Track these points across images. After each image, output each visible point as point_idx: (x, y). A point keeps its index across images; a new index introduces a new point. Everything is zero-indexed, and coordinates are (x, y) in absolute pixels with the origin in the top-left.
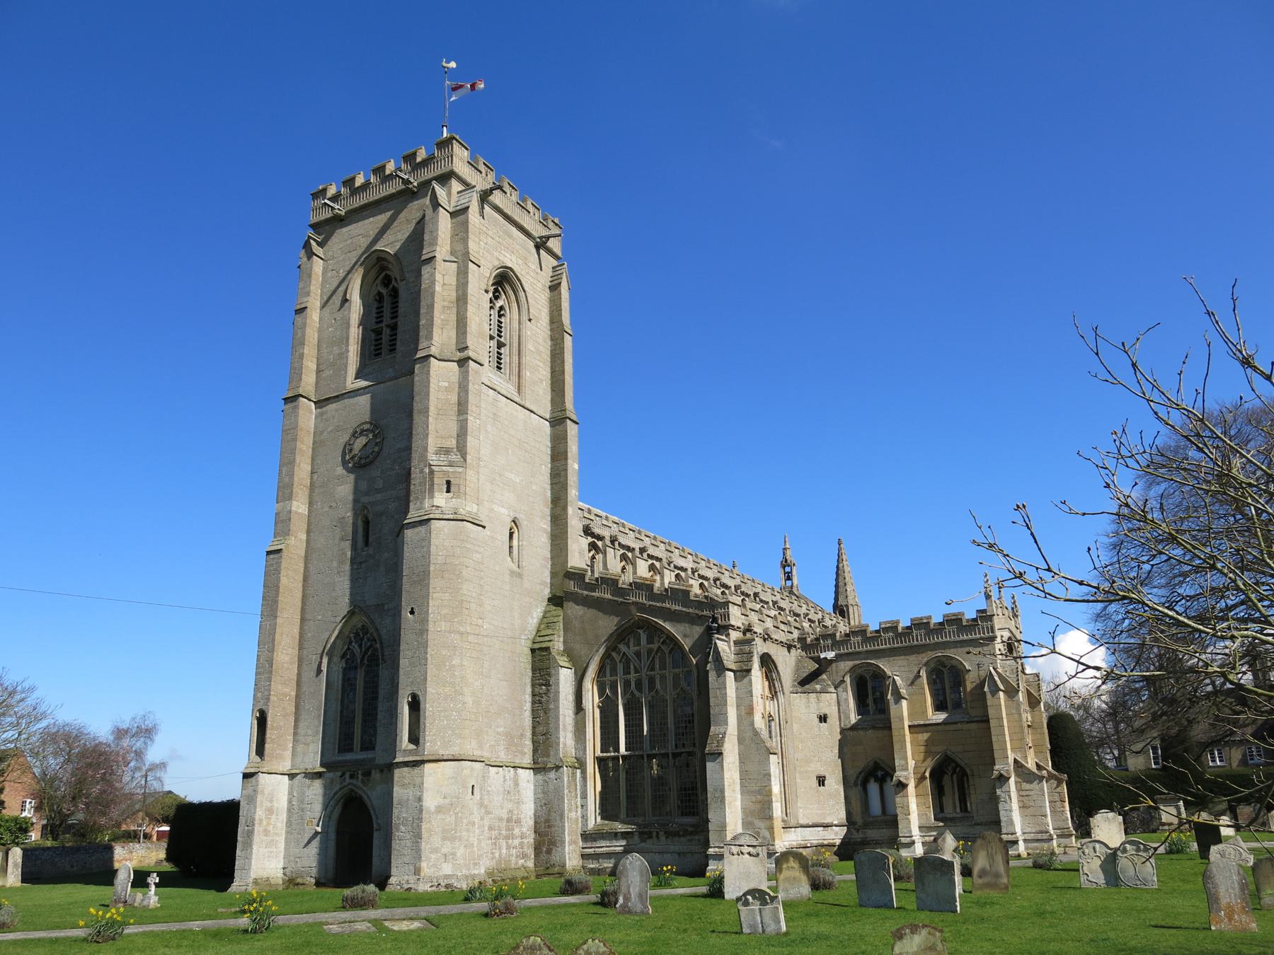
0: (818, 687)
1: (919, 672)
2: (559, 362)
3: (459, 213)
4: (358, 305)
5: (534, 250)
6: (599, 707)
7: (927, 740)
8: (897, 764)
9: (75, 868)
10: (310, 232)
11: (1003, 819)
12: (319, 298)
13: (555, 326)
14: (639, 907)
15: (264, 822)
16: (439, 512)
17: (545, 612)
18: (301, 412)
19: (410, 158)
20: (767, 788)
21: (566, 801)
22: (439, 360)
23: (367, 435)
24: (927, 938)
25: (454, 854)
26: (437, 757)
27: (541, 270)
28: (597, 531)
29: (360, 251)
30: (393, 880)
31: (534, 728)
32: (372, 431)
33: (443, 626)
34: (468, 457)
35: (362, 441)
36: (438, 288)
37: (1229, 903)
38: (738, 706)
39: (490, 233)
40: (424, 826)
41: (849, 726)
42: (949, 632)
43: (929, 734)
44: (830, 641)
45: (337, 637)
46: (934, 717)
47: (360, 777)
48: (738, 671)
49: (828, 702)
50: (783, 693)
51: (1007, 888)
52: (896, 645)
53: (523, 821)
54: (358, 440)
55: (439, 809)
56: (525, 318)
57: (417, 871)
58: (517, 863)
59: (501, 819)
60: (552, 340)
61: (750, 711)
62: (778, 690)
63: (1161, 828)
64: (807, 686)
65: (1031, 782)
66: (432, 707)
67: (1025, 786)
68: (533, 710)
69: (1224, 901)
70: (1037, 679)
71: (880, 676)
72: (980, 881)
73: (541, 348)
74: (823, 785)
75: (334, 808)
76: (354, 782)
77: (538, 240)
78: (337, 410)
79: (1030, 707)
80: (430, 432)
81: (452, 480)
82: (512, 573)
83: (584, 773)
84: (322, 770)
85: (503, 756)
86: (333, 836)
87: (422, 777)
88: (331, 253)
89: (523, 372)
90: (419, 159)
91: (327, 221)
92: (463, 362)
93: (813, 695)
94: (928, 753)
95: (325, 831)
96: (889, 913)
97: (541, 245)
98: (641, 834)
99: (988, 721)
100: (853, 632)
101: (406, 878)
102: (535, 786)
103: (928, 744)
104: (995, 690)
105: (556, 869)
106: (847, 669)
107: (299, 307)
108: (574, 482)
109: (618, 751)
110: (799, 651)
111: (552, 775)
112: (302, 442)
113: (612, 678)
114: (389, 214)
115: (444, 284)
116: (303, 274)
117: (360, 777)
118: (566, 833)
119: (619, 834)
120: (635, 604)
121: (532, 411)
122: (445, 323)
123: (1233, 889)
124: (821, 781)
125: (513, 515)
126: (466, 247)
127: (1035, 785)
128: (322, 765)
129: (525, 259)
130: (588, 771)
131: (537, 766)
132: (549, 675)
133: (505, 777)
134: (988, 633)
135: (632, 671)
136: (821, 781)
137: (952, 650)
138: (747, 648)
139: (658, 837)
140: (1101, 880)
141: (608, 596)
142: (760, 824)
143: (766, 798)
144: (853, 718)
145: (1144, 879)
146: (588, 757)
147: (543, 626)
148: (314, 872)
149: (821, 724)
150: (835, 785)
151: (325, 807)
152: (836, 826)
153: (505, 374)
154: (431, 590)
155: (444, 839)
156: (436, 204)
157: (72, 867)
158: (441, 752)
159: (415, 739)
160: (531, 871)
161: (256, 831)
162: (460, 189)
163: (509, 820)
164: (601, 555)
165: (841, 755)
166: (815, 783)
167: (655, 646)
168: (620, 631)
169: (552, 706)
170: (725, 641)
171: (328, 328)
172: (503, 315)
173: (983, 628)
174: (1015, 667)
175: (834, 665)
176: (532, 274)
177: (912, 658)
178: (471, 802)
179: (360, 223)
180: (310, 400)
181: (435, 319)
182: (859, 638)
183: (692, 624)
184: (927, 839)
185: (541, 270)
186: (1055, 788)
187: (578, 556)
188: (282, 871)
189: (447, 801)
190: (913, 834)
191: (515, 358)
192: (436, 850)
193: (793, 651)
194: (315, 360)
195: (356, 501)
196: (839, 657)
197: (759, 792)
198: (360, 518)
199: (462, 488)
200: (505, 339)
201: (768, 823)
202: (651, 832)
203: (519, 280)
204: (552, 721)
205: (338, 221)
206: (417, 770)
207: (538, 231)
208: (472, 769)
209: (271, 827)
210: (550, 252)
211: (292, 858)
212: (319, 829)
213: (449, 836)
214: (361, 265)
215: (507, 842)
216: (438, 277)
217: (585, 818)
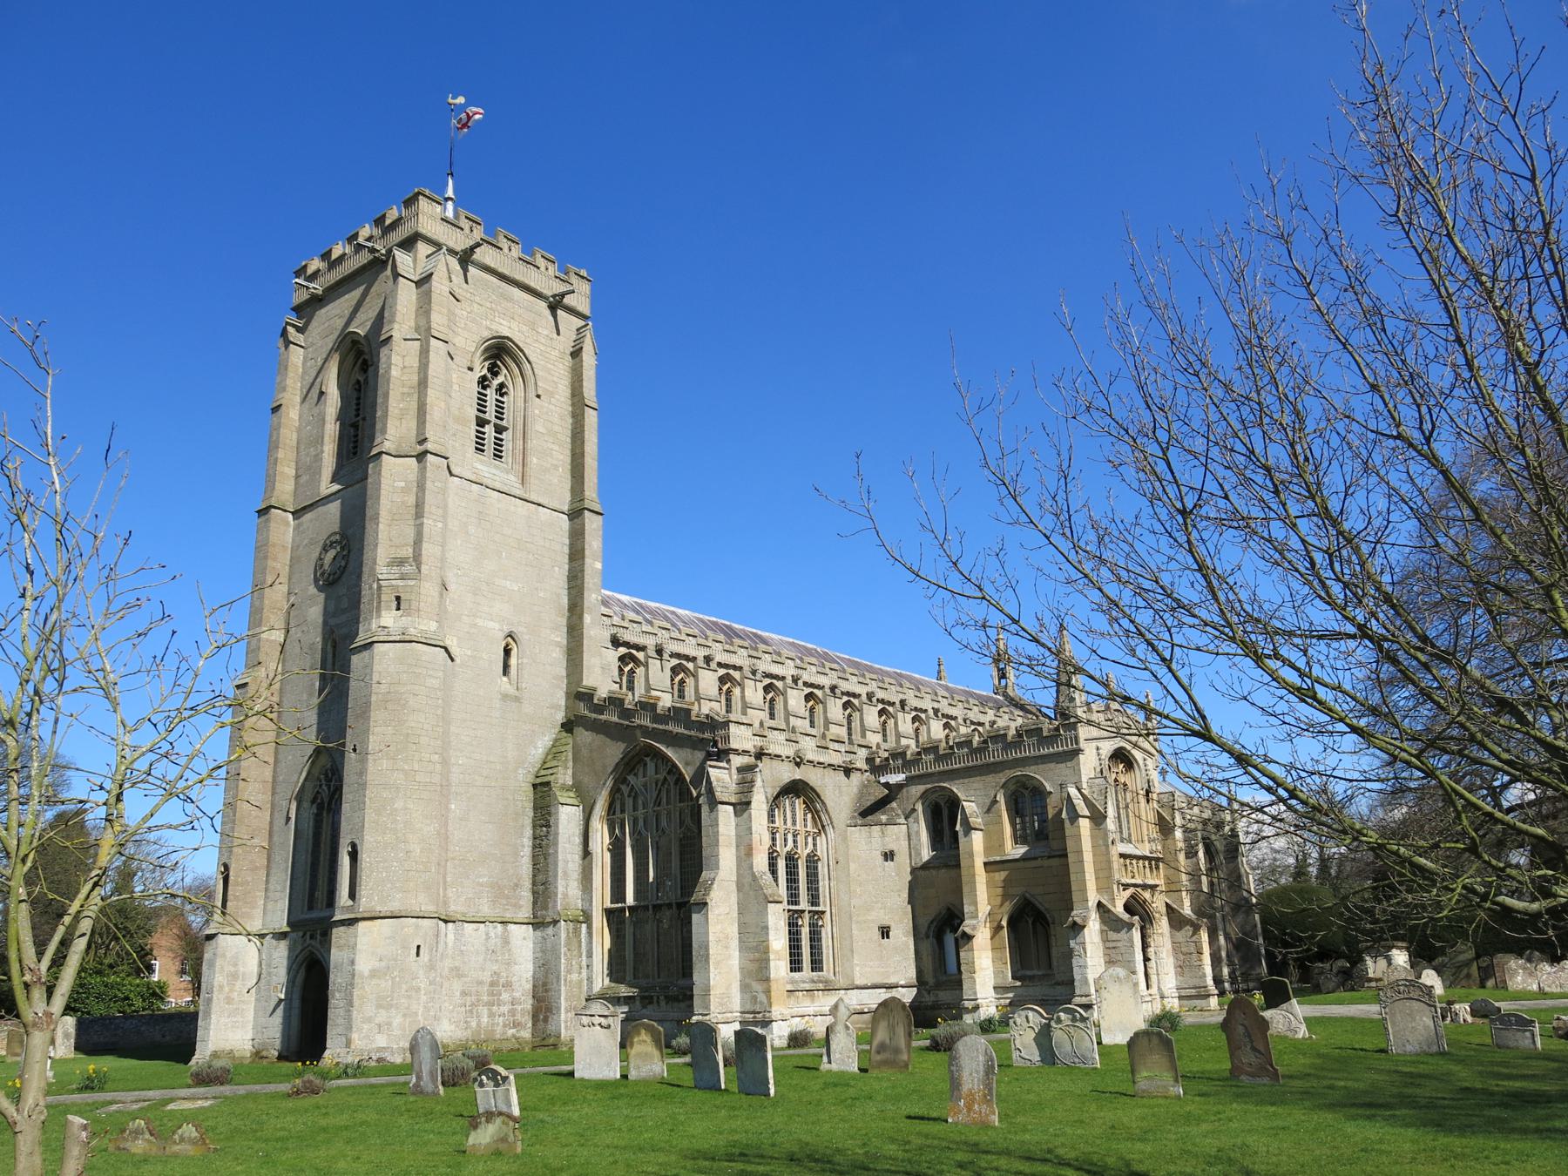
0: (884, 818)
1: (995, 797)
2: (579, 442)
3: (424, 281)
4: (335, 397)
5: (547, 312)
6: (609, 849)
7: (1004, 881)
8: (966, 911)
9: (168, 1038)
10: (292, 318)
11: (1077, 977)
12: (299, 392)
13: (576, 399)
14: (430, 1088)
15: (226, 989)
16: (385, 633)
17: (556, 740)
18: (272, 525)
19: (379, 221)
20: (765, 944)
21: (563, 961)
22: (395, 456)
23: (335, 548)
24: (500, 1128)
25: (389, 1024)
26: (373, 915)
27: (558, 334)
28: (627, 636)
29: (337, 333)
30: (327, 1054)
31: (534, 876)
32: (340, 543)
33: (385, 764)
34: (424, 568)
35: (331, 554)
36: (394, 372)
37: (970, 1090)
38: (737, 846)
39: (477, 299)
40: (356, 993)
41: (919, 865)
42: (1029, 745)
43: (1006, 873)
44: (900, 762)
45: (306, 779)
46: (1014, 852)
47: (318, 937)
48: (738, 804)
49: (896, 836)
50: (833, 827)
51: (906, 1066)
52: (971, 764)
53: (516, 986)
54: (328, 554)
55: (374, 974)
56: (532, 394)
57: (348, 1044)
58: (504, 1033)
59: (480, 983)
60: (573, 417)
61: (749, 852)
62: (825, 823)
63: (1366, 985)
64: (869, 817)
65: (1118, 931)
66: (370, 857)
67: (1112, 935)
68: (533, 856)
69: (965, 1088)
70: (1171, 798)
71: (954, 804)
72: (878, 1058)
73: (556, 428)
74: (888, 937)
75: (298, 972)
76: (313, 943)
77: (551, 299)
78: (311, 521)
79: (1162, 834)
80: (380, 541)
81: (402, 595)
82: (505, 697)
83: (590, 928)
84: (288, 929)
85: (486, 910)
86: (296, 1003)
87: (356, 937)
88: (310, 340)
89: (528, 459)
90: (388, 222)
91: (307, 303)
92: (421, 457)
93: (877, 828)
94: (1005, 896)
95: (288, 1000)
96: (716, 1094)
97: (556, 304)
98: (643, 998)
99: (1066, 856)
100: (924, 749)
101: (338, 1050)
102: (534, 943)
103: (1007, 884)
104: (1074, 816)
105: (551, 1041)
106: (919, 794)
107: (275, 405)
108: (594, 584)
109: (624, 901)
110: (868, 774)
111: (550, 930)
112: (275, 559)
113: (622, 816)
114: (363, 287)
115: (405, 367)
116: (282, 367)
117: (318, 937)
118: (562, 998)
119: (622, 999)
120: (641, 726)
121: (539, 505)
122: (403, 414)
123: (977, 1072)
124: (885, 932)
125: (506, 630)
126: (429, 322)
127: (1123, 935)
128: (289, 924)
129: (533, 326)
130: (594, 926)
131: (537, 921)
132: (549, 814)
133: (487, 934)
134: (1072, 745)
135: (641, 807)
136: (885, 932)
137: (1032, 767)
138: (749, 776)
139: (658, 1002)
140: (1036, 1057)
141: (615, 719)
142: (757, 987)
143: (764, 956)
144: (926, 854)
145: (1082, 1055)
146: (594, 909)
147: (550, 757)
148: (278, 1044)
149: (886, 863)
150: (903, 937)
151: (289, 970)
152: (902, 987)
153: (507, 463)
154: (371, 723)
155: (379, 1006)
156: (396, 275)
157: (164, 1036)
158: (378, 908)
159: (352, 895)
160: (526, 1042)
161: (215, 998)
162: (430, 252)
163: (492, 984)
164: (642, 668)
165: (912, 900)
166: (877, 934)
167: (661, 777)
168: (626, 760)
169: (551, 851)
170: (724, 768)
171: (306, 427)
172: (506, 393)
173: (1066, 739)
174: (1104, 787)
175: (905, 790)
176: (543, 341)
177: (990, 778)
178: (417, 966)
179: (337, 302)
180: (286, 511)
181: (390, 409)
182: (932, 756)
183: (694, 749)
184: (1002, 1002)
185: (558, 334)
186: (1192, 936)
187: (601, 675)
188: (251, 1043)
189: (383, 964)
190: (979, 996)
191: (520, 443)
192: (369, 1020)
193: (855, 776)
194: (293, 464)
195: (325, 623)
196: (911, 781)
197: (756, 949)
198: (329, 644)
199: (414, 605)
200: (508, 421)
201: (765, 985)
202: (652, 997)
203: (522, 351)
204: (551, 867)
205: (316, 302)
206: (352, 929)
207: (552, 287)
208: (417, 926)
209: (236, 994)
210: (571, 311)
211: (259, 1029)
212: (283, 997)
213: (383, 1004)
214: (336, 351)
215: (489, 1009)
216: (395, 359)
217: (590, 979)
